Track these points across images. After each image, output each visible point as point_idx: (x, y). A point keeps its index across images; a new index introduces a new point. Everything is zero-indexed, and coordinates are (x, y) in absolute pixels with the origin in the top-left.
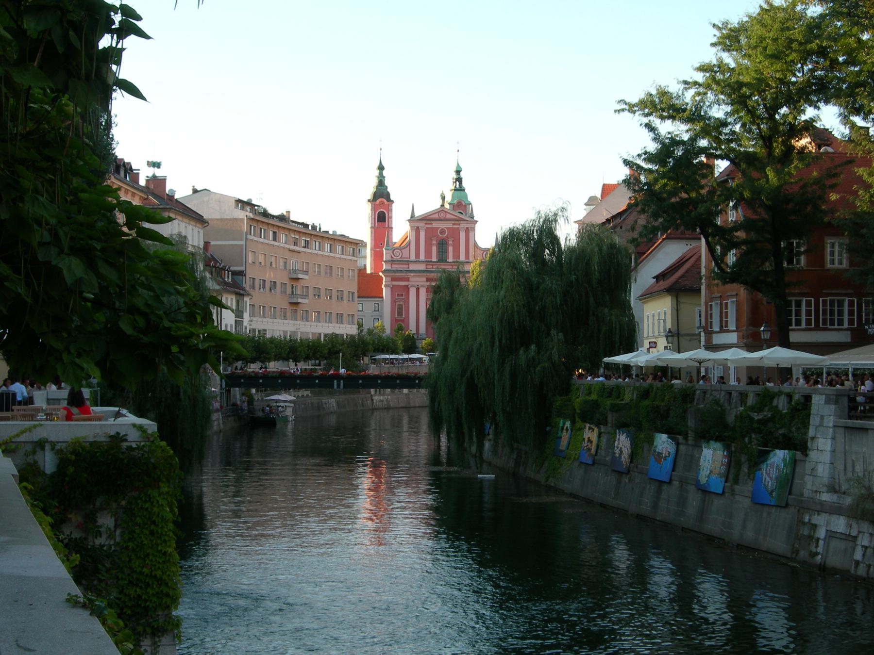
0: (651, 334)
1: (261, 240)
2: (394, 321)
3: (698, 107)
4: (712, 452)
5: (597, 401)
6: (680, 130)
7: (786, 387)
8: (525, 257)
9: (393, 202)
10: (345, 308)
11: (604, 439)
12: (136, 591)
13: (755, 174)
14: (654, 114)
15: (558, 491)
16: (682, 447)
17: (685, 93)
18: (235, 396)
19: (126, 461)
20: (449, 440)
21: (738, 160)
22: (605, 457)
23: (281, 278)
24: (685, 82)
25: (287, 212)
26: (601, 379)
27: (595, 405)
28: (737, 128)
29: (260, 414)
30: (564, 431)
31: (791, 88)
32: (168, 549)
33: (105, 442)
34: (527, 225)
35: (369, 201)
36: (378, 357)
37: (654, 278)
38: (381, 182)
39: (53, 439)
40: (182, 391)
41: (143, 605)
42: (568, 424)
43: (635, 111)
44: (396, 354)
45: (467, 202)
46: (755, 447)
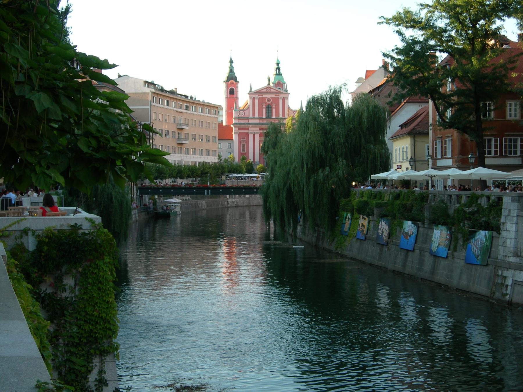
0: (398, 161)
1: (160, 106)
2: (240, 154)
3: (428, 21)
4: (440, 232)
5: (367, 201)
6: (418, 34)
7: (486, 192)
8: (322, 114)
9: (238, 82)
10: (211, 146)
11: (372, 224)
12: (89, 327)
13: (464, 62)
14: (402, 25)
15: (342, 256)
16: (420, 229)
17: (421, 12)
18: (145, 200)
19: (81, 242)
20: (275, 225)
21: (453, 53)
22: (373, 235)
23: (172, 128)
24: (422, 5)
25: (175, 88)
26: (369, 188)
27: (366, 203)
28: (453, 33)
29: (160, 211)
30: (347, 219)
31: (486, 8)
32: (109, 299)
33: (68, 230)
34: (323, 94)
35: (224, 82)
36: (231, 176)
37: (399, 126)
38: (231, 71)
39: (33, 228)
40: (114, 197)
41: (94, 336)
42: (349, 215)
43: (390, 23)
44: (242, 174)
45: (283, 82)
46: (467, 229)
